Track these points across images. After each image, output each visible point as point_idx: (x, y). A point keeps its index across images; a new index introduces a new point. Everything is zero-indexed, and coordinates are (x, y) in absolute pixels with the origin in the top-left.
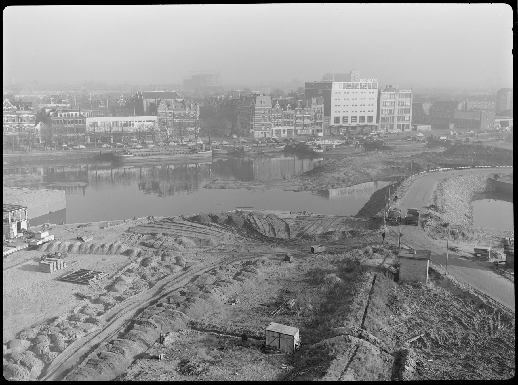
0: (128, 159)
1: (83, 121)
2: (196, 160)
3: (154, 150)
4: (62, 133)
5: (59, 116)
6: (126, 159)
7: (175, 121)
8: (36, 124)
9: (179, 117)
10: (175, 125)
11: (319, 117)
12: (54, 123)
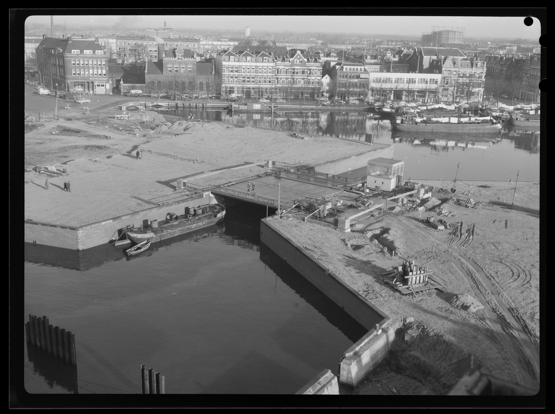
7: (459, 80)
9: (464, 76)
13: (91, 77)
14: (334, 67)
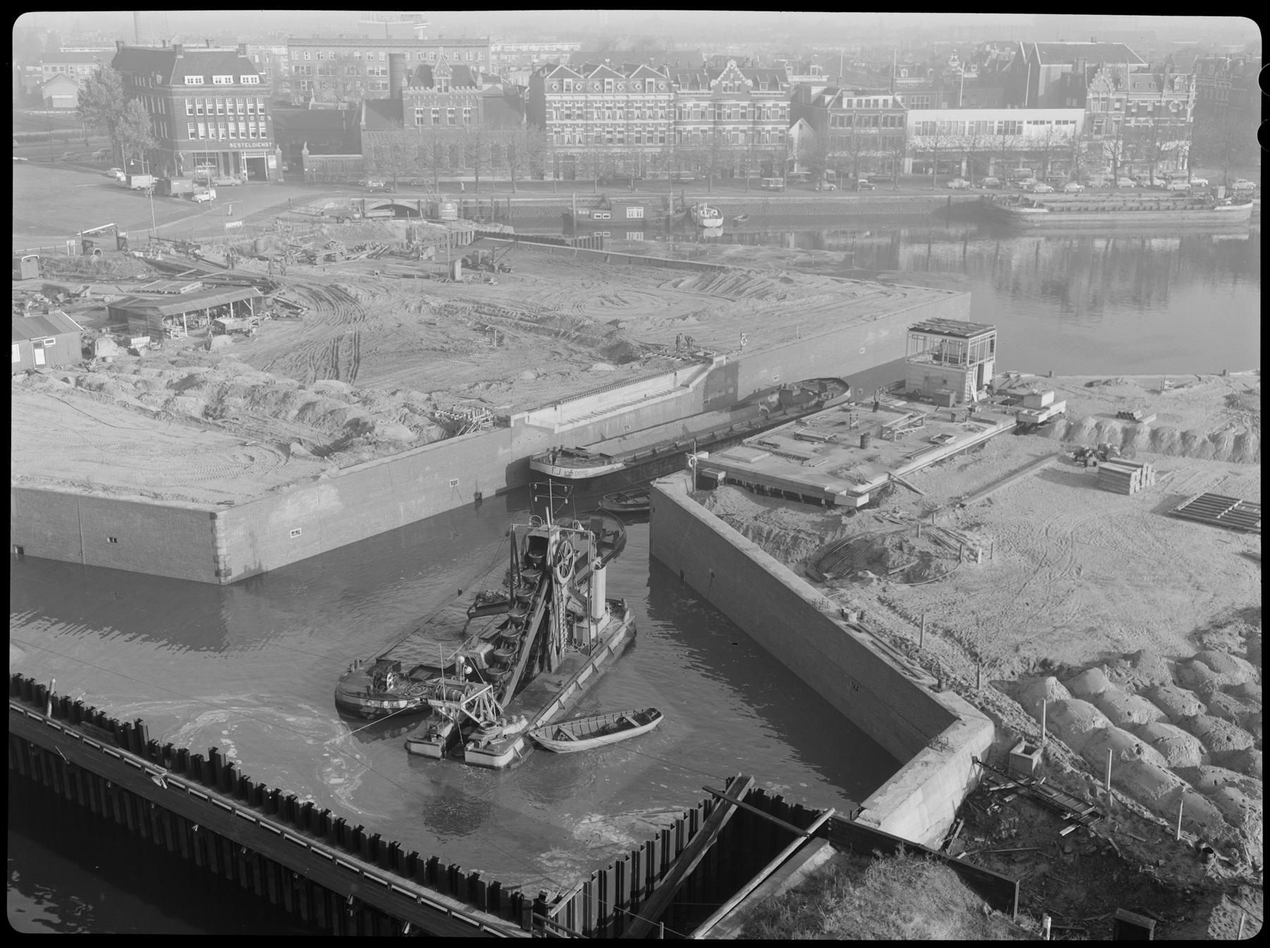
0: (1034, 218)
1: (901, 119)
2: (1207, 226)
3: (1080, 197)
4: (859, 149)
5: (845, 106)
6: (1029, 218)
8: (792, 124)
9: (1142, 111)
10: (1126, 134)
11: (302, 99)
12: (834, 124)
13: (233, 141)
14: (820, 99)
